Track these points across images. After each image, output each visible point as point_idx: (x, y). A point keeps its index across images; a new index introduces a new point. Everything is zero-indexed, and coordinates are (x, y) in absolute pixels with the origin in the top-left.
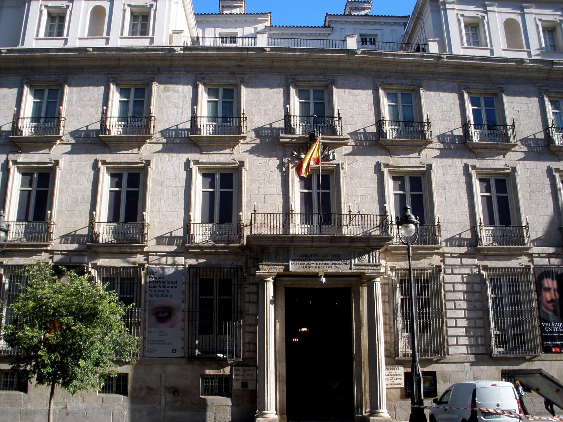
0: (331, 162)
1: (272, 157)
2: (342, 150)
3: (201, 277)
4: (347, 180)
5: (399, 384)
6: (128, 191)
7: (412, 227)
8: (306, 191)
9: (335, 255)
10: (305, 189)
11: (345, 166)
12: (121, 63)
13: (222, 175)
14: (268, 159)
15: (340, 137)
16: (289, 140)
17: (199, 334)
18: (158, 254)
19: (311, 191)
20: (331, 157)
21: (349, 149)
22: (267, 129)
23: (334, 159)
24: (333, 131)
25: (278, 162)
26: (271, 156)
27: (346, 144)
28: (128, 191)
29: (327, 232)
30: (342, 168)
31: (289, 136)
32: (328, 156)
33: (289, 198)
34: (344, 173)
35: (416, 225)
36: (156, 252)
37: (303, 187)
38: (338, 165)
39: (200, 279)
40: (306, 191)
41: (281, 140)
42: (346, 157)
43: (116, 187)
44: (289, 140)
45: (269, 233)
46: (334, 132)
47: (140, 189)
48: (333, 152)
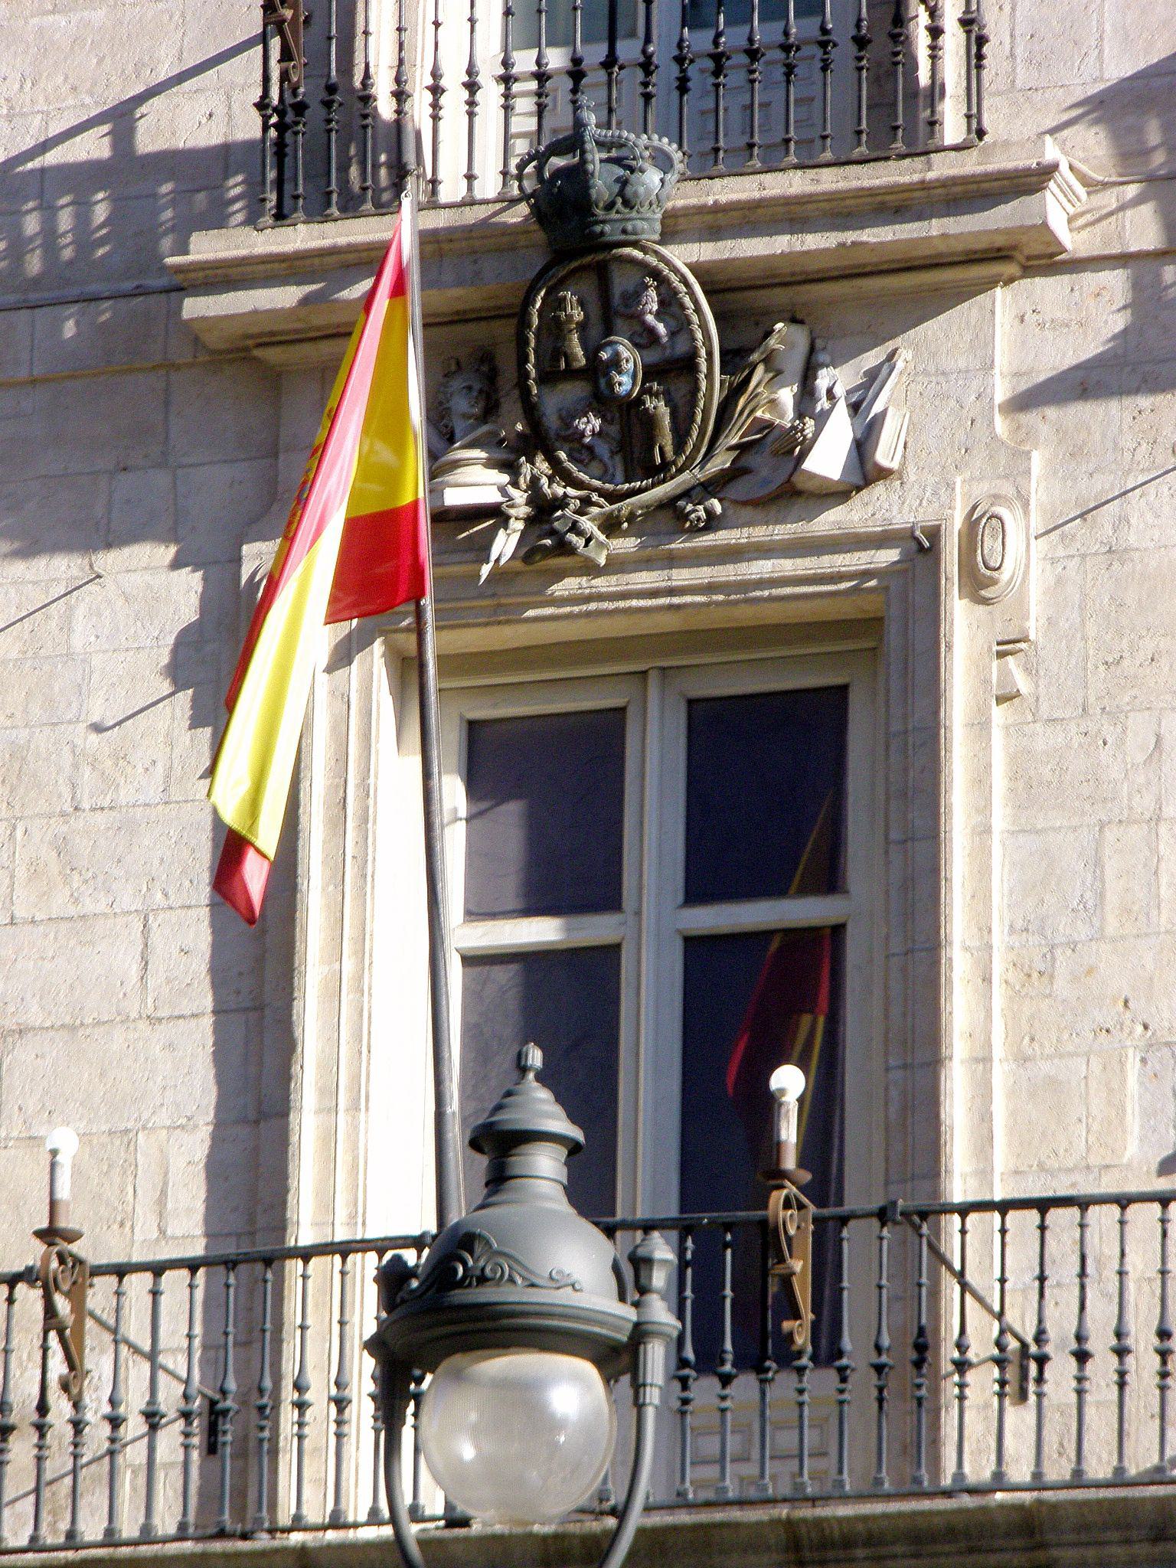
0: (831, 520)
1: (111, 539)
2: (983, 343)
4: (1045, 739)
6: (697, 947)
7: (572, 1390)
8: (542, 931)
10: (534, 907)
11: (1021, 554)
13: (713, 726)
14: (63, 567)
15: (969, 165)
16: (286, 297)
19: (596, 930)
20: (828, 458)
21: (1085, 315)
22: (82, 179)
23: (865, 470)
24: (883, 105)
25: (183, 595)
26: (99, 533)
27: (1043, 259)
28: (697, 947)
29: (784, 1450)
30: (978, 583)
31: (300, 237)
32: (791, 447)
33: (287, 1046)
34: (1007, 647)
35: (617, 1358)
37: (510, 888)
38: (922, 548)
40: (542, 931)
41: (195, 307)
42: (1049, 419)
43: (532, 909)
44: (286, 297)
45: (92, 1529)
46: (895, 112)
47: (857, 906)
48: (873, 379)
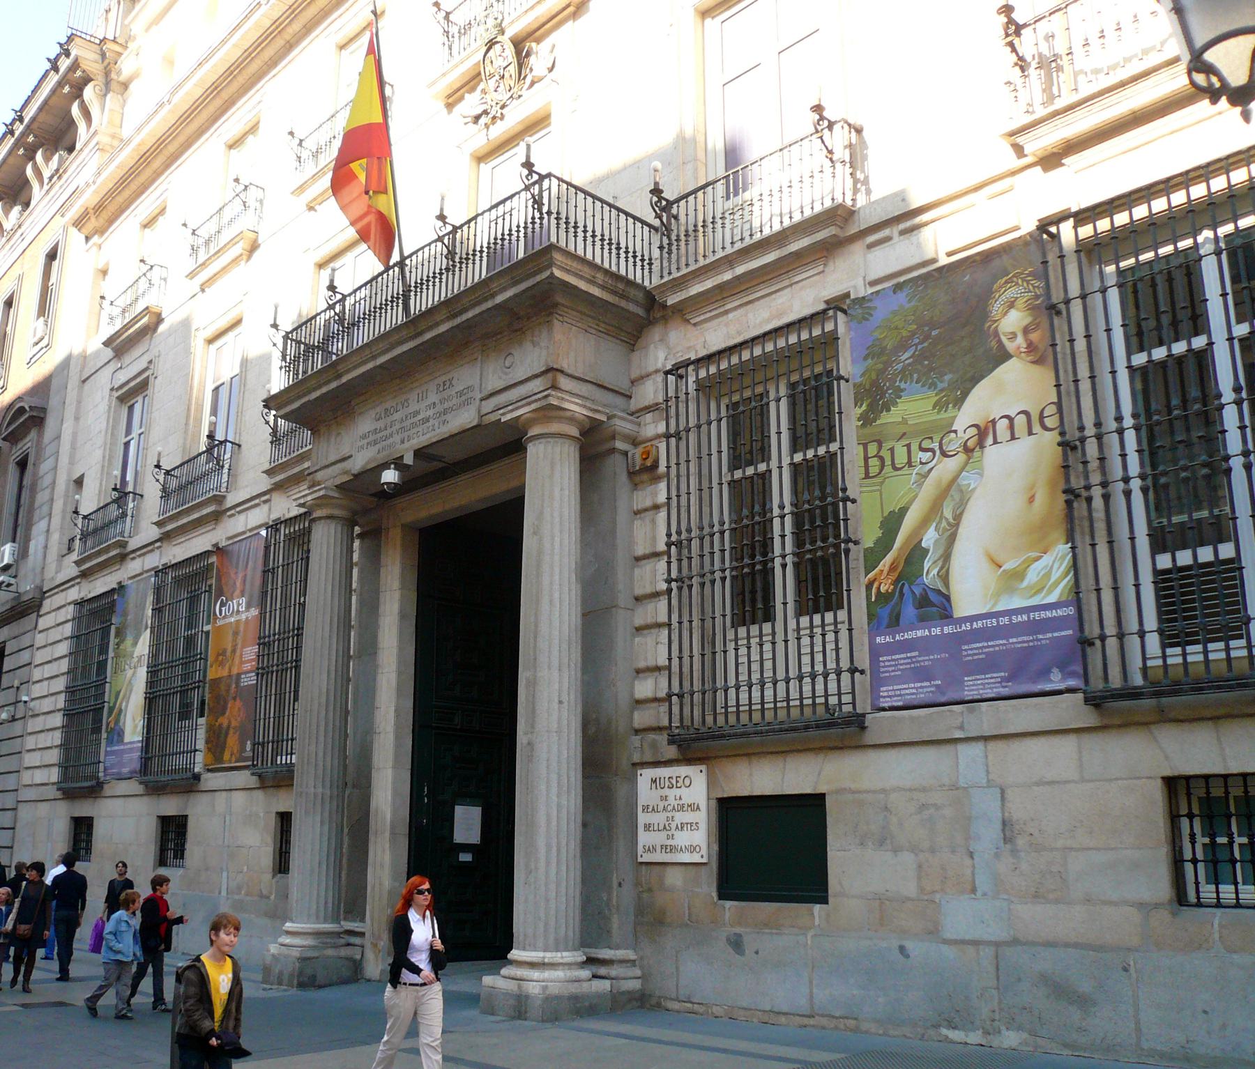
5: (692, 849)
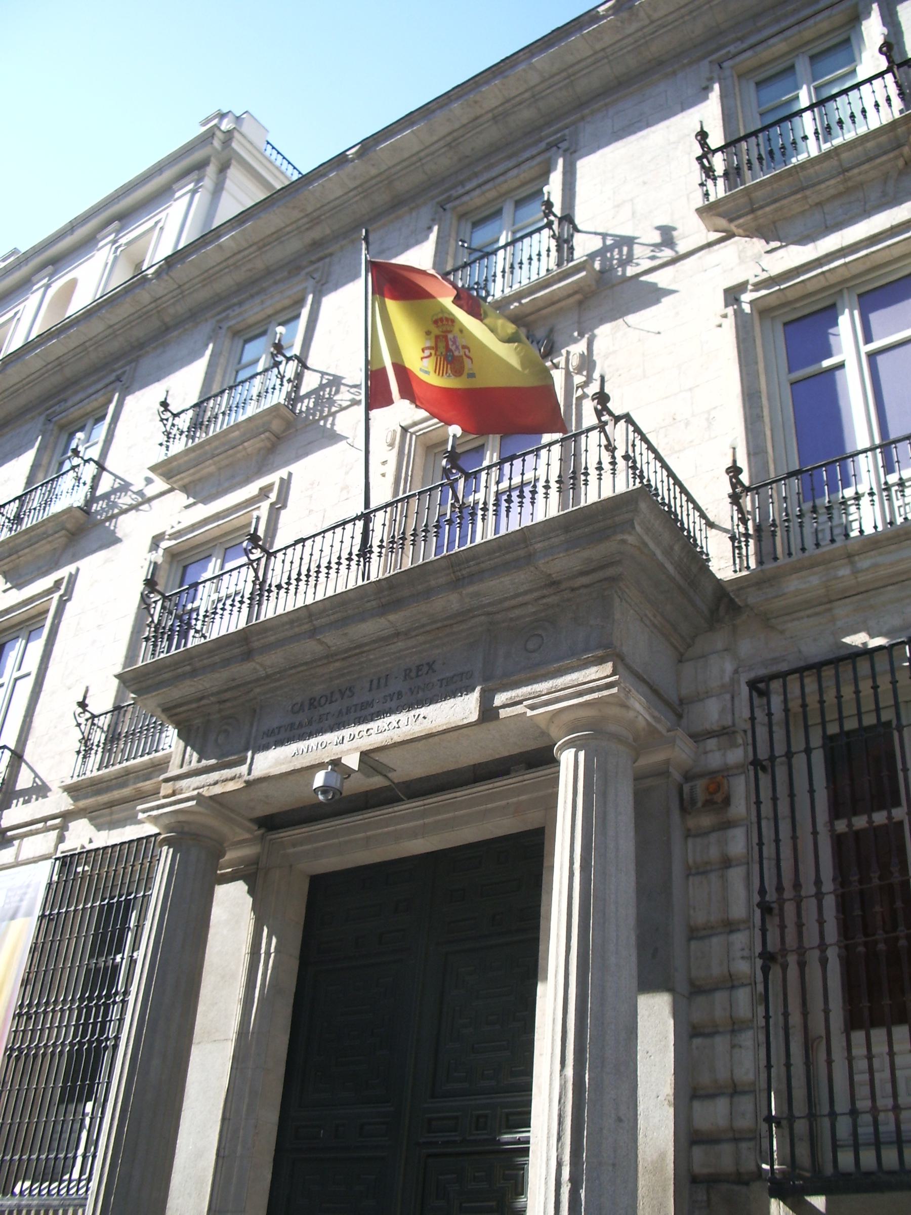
3: (833, 729)
9: (419, 668)
12: (68, 372)
17: (853, 1022)
18: (50, 823)
36: (45, 820)
39: (828, 740)
